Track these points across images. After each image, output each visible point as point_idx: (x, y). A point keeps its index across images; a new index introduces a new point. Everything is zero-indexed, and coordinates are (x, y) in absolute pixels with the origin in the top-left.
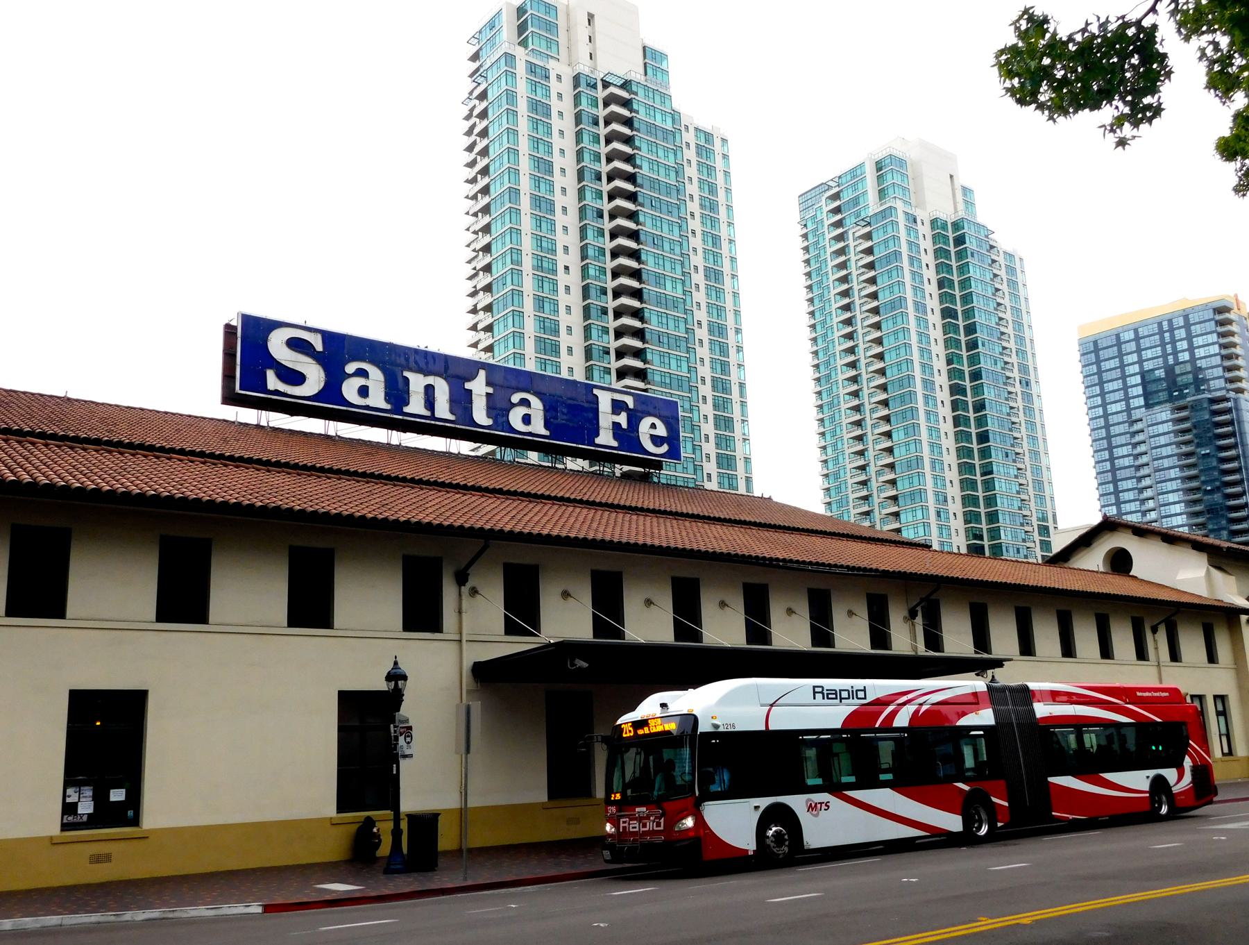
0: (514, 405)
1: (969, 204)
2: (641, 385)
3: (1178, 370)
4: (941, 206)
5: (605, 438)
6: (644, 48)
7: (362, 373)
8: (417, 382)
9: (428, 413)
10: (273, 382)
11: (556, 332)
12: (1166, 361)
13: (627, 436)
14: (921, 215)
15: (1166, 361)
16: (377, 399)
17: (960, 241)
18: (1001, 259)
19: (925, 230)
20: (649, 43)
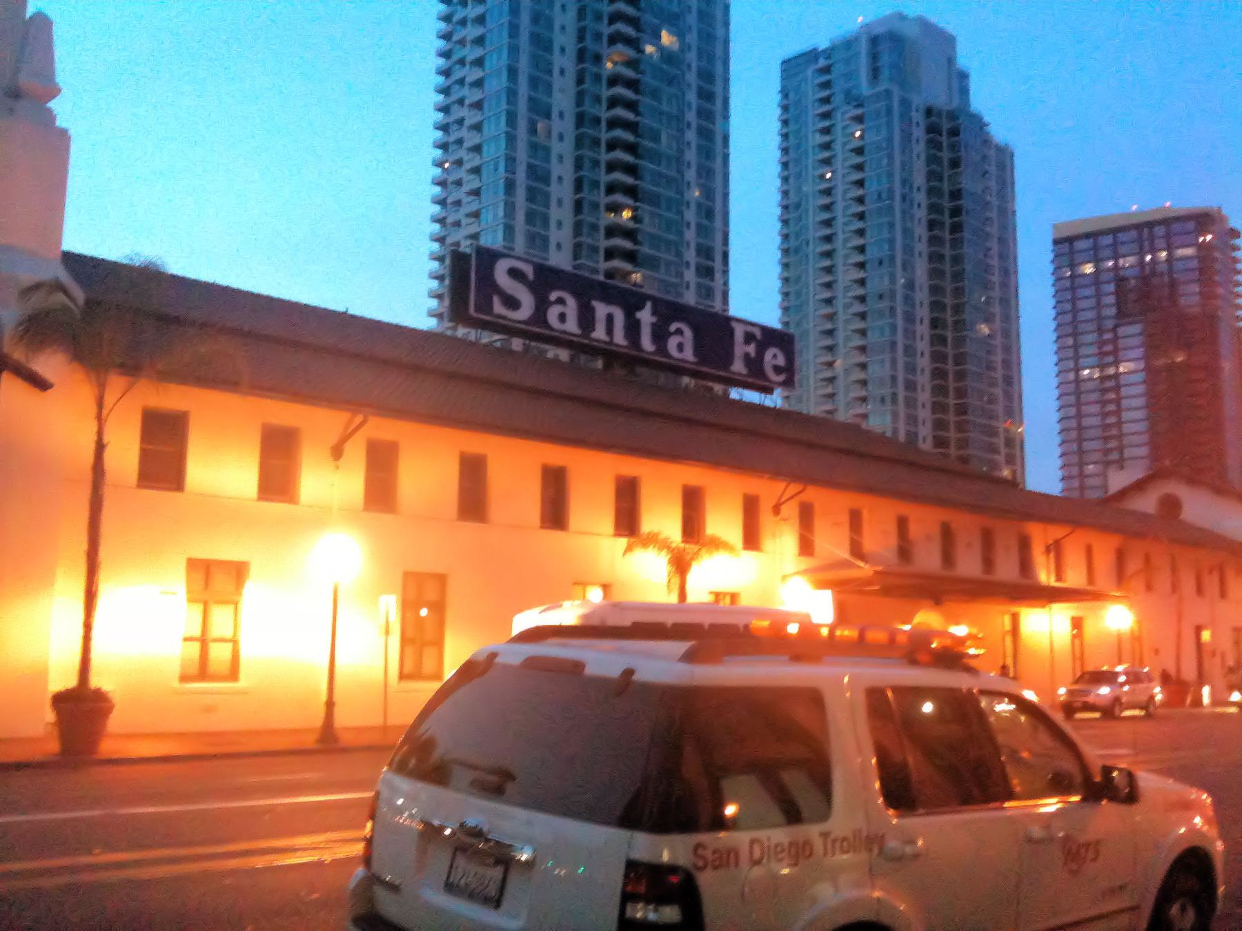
0: (671, 334)
1: (964, 91)
5: (738, 366)
7: (561, 301)
8: (601, 310)
9: (607, 339)
10: (498, 307)
11: (547, 159)
16: (572, 326)
18: (992, 153)
19: (918, 116)
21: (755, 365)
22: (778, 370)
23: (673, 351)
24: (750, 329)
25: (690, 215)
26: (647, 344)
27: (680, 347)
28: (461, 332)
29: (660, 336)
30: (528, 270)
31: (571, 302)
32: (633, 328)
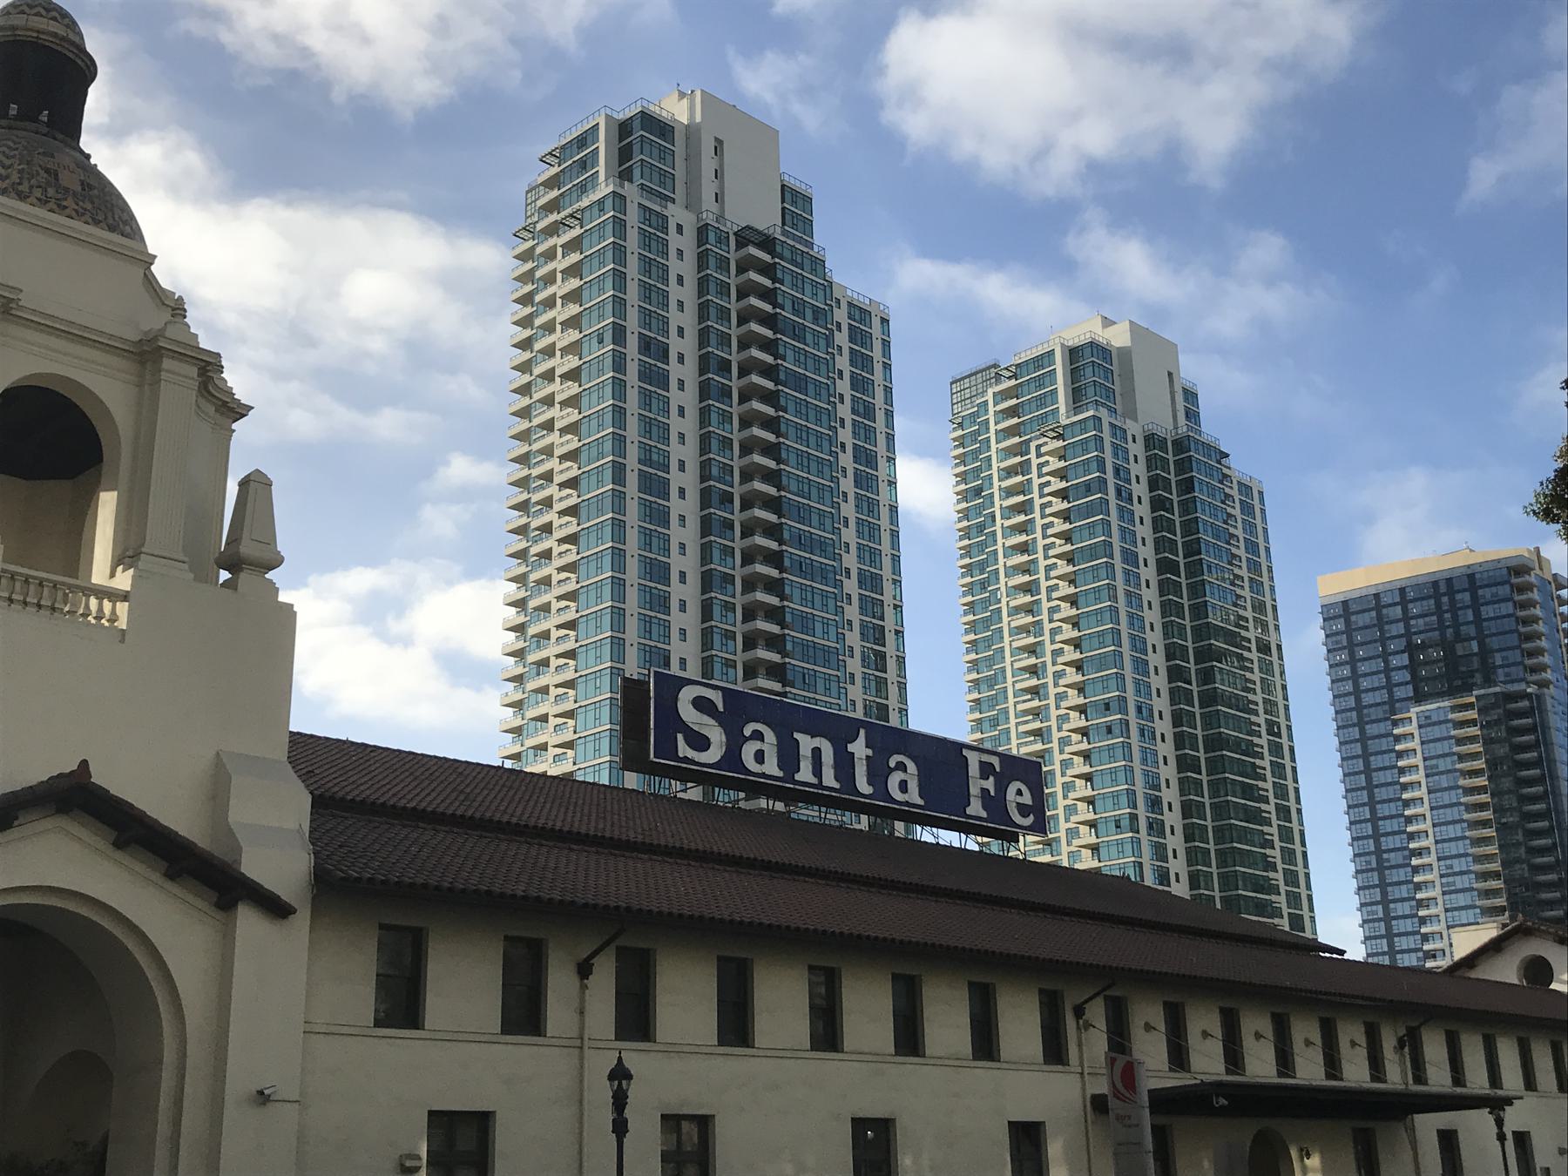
0: (747, 739)
1: (1192, 415)
2: (777, 687)
3: (1460, 650)
4: (1155, 411)
5: (975, 808)
6: (783, 186)
8: (806, 743)
9: (814, 781)
10: (684, 749)
12: (1443, 634)
13: (995, 803)
14: (1132, 428)
15: (1443, 634)
16: (771, 767)
17: (1184, 465)
19: (1137, 449)
20: (791, 182)
21: (995, 803)
22: (1023, 810)
23: (751, 765)
24: (985, 758)
25: (851, 586)
26: (863, 786)
27: (903, 786)
28: (632, 780)
29: (878, 774)
30: (716, 697)
31: (770, 736)
32: (845, 764)
